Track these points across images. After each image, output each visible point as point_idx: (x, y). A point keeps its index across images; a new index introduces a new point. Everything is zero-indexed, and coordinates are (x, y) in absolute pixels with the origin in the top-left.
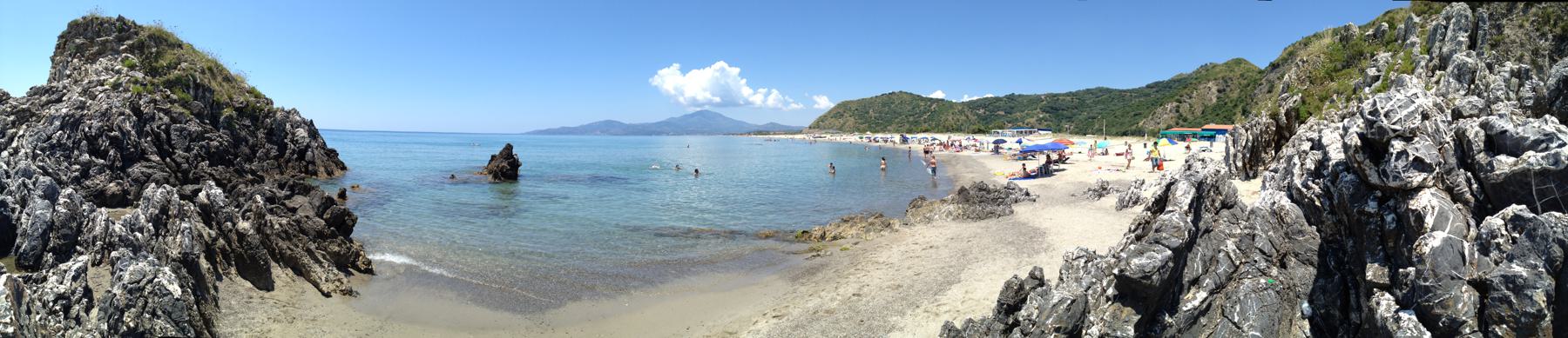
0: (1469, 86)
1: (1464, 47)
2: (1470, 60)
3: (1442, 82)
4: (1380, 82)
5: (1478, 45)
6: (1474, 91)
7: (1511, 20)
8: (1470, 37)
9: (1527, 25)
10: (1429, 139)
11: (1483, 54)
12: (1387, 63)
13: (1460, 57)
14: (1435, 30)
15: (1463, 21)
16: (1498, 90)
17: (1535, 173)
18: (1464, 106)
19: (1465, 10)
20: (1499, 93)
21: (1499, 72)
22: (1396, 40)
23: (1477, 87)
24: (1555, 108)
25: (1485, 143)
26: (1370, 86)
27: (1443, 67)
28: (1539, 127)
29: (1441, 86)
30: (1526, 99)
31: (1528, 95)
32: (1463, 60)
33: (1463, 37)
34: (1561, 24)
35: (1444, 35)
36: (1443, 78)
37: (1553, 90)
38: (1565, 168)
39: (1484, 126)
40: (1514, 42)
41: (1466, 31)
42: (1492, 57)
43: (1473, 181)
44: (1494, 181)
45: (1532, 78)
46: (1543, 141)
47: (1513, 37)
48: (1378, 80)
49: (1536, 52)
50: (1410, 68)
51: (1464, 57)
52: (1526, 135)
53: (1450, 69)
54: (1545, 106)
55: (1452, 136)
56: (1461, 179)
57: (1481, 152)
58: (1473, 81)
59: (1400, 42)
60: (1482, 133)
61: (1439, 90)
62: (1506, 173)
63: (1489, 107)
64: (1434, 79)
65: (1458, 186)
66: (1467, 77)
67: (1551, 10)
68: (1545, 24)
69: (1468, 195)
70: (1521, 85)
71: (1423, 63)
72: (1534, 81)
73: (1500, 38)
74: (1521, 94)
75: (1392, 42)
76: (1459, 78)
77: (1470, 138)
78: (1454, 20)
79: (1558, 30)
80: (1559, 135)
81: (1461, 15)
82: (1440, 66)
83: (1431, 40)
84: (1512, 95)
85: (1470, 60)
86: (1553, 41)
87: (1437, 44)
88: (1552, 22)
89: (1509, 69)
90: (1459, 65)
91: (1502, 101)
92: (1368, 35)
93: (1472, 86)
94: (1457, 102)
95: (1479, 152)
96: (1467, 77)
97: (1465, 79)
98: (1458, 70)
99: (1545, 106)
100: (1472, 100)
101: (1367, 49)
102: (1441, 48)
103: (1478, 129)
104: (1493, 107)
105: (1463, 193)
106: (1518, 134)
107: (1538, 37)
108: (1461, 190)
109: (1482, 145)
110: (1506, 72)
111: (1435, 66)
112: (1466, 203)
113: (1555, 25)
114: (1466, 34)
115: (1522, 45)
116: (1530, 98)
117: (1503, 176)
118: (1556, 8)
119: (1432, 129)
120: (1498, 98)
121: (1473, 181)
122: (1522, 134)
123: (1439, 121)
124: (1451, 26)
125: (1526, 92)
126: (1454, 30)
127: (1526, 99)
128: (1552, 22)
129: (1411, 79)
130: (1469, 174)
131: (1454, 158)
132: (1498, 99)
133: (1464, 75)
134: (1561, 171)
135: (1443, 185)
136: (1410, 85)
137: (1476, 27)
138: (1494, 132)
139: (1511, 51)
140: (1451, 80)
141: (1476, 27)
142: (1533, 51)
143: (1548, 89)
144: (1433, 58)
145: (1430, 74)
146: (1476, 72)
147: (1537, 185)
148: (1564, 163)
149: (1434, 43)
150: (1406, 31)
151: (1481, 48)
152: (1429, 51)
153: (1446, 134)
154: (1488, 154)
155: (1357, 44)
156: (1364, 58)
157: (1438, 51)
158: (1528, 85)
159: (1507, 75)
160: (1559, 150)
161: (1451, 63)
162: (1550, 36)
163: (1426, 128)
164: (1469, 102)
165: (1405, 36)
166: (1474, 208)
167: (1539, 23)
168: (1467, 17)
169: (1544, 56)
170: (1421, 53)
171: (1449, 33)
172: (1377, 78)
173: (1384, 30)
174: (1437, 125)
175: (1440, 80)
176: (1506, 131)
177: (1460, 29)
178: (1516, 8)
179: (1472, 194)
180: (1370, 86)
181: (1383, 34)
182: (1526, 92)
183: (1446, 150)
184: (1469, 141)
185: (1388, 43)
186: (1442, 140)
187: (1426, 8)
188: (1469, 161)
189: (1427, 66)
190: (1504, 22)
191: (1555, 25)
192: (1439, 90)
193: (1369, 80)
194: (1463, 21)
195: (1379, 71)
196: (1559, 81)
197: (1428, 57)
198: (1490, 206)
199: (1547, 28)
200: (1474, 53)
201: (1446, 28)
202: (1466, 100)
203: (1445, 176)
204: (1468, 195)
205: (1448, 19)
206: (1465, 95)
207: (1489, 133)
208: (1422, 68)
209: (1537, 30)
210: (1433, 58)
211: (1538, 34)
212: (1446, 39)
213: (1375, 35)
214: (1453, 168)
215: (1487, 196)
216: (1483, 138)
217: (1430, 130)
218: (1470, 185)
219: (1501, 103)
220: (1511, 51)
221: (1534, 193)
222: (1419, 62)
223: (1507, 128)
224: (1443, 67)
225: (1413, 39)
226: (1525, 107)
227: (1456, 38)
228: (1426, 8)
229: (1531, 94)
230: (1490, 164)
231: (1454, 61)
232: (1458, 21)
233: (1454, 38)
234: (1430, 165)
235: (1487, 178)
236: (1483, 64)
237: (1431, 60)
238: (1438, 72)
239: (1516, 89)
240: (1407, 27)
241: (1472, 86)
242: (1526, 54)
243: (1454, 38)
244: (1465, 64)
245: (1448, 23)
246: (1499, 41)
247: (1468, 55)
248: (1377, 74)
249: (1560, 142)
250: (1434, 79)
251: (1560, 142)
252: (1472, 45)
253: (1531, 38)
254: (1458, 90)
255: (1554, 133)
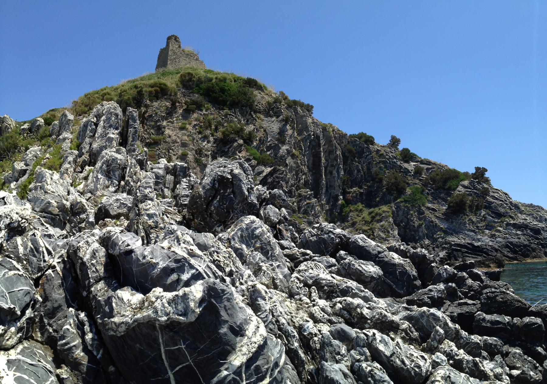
0: (120, 182)
1: (114, 143)
2: (119, 156)
3: (90, 178)
4: (26, 176)
5: (130, 142)
6: (124, 187)
7: (172, 123)
8: (121, 134)
9: (190, 128)
10: (19, 266)
11: (134, 150)
12: (36, 157)
13: (110, 153)
14: (86, 126)
15: (113, 119)
16: (145, 188)
17: (161, 325)
18: (111, 204)
19: (115, 109)
20: (147, 191)
21: (152, 169)
22: (50, 136)
23: (127, 183)
24: (213, 208)
25: (106, 266)
26: (17, 181)
27: (92, 163)
28: (169, 248)
29: (89, 182)
30: (183, 197)
31: (184, 193)
32: (112, 156)
33: (114, 134)
34: (221, 129)
35: (94, 131)
36: (91, 174)
37: (208, 190)
38: (197, 319)
39: (106, 241)
40: (175, 142)
41: (117, 129)
42: (144, 154)
43: (87, 328)
44: (112, 333)
45: (190, 176)
46: (173, 271)
47: (174, 138)
48: (24, 174)
49: (199, 152)
50: (58, 163)
51: (113, 153)
52: (154, 261)
53: (99, 164)
54: (202, 205)
55: (61, 256)
56: (70, 327)
57: (100, 280)
58: (123, 178)
59: (54, 137)
60: (102, 252)
61: (87, 186)
62: (126, 323)
63: (137, 206)
64: (82, 175)
65: (63, 337)
66: (117, 173)
67: (212, 117)
68: (207, 128)
69: (79, 353)
70: (177, 182)
71: (71, 159)
72: (192, 179)
73: (161, 137)
74: (177, 191)
75: (46, 136)
76: (108, 174)
77: (85, 259)
78: (104, 118)
79: (219, 135)
80: (193, 261)
81: (111, 113)
82: (90, 162)
83: (81, 136)
84: (167, 192)
85: (119, 156)
86: (214, 143)
87: (87, 140)
88: (213, 127)
89: (163, 166)
90: (107, 161)
91: (152, 200)
92: (23, 129)
93: (123, 183)
94: (104, 200)
95: (97, 281)
96: (117, 173)
97: (115, 175)
98: (107, 166)
99: (202, 205)
100: (120, 198)
101: (20, 140)
102: (91, 144)
103: (96, 245)
104: (141, 206)
105: (70, 348)
106: (144, 257)
107: (201, 139)
108: (66, 344)
109: (101, 269)
110: (160, 168)
111: (84, 161)
112: (74, 365)
113: (216, 130)
114: (116, 131)
115: (184, 145)
116: (187, 196)
117: (123, 328)
118: (216, 116)
119: (25, 248)
120: (146, 196)
121: (87, 328)
122: (148, 258)
123: (38, 237)
124: (102, 123)
125: (183, 188)
126: (104, 127)
127: (183, 197)
128: (213, 127)
129: (52, 175)
130: (82, 315)
131: (61, 291)
132: (146, 198)
133: (114, 171)
134: (191, 324)
135: (42, 334)
136: (49, 181)
137: (127, 125)
138: (116, 252)
139: (172, 150)
140: (100, 176)
141: (127, 125)
142: (196, 151)
143: (204, 188)
144: (83, 154)
145: (79, 169)
146: (126, 168)
147: (166, 345)
148: (194, 311)
149: (83, 139)
150: (60, 127)
151: (133, 145)
152: (79, 147)
153: (49, 253)
154: (109, 285)
155: (12, 137)
156: (19, 152)
157: (87, 147)
158: (184, 183)
159: (161, 172)
160: (187, 289)
161: (100, 158)
162: (211, 139)
163: (16, 247)
164: (117, 200)
165: (59, 132)
166: (87, 373)
167: (201, 127)
168: (117, 115)
169: (206, 156)
170: (71, 149)
171: (100, 130)
172: (23, 172)
173: (39, 125)
174: (34, 242)
175: (88, 176)
176: (132, 251)
177: (110, 126)
178: (175, 112)
179: (85, 349)
180: (17, 181)
181: (38, 129)
182: (183, 188)
183: (49, 279)
184: (83, 264)
185: (42, 138)
186: (42, 264)
187: (86, 109)
188: (85, 294)
189: (75, 161)
190: (165, 123)
191: (216, 130)
192: (87, 186)
193: (16, 174)
194: (113, 119)
195: (27, 165)
196: (214, 180)
197: (76, 152)
198: (112, 369)
199: (208, 132)
200: (124, 150)
201: (96, 125)
202: (114, 198)
203: (46, 321)
204: (79, 353)
205: (98, 116)
206: (115, 192)
207: (111, 252)
208: (69, 163)
209: (200, 133)
210: (83, 154)
211: (200, 136)
212: (96, 135)
213: (30, 130)
214: (60, 306)
215: (107, 352)
216: (103, 259)
217: (21, 250)
218: (83, 335)
219: (150, 202)
220: (172, 150)
221: (164, 357)
222: (67, 157)
223: (132, 247)
224: (92, 163)
225: (66, 135)
226: (182, 205)
227: (106, 134)
228: (86, 109)
229: (187, 192)
230: (109, 301)
231: (103, 157)
232: (108, 119)
233: (104, 135)
234: (11, 311)
235: (104, 324)
236: (134, 161)
237: (80, 155)
238: (87, 168)
239: (172, 186)
240: (61, 123)
241: (123, 183)
242: (189, 153)
243: (104, 135)
244: (115, 160)
245: (98, 120)
246: (160, 140)
247: (118, 151)
248: (24, 167)
249: (194, 271)
250: (82, 175)
251: (194, 271)
252: (123, 142)
253: (194, 139)
254: (108, 187)
255: (184, 258)
